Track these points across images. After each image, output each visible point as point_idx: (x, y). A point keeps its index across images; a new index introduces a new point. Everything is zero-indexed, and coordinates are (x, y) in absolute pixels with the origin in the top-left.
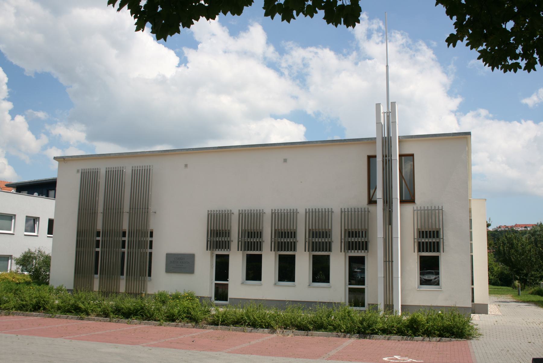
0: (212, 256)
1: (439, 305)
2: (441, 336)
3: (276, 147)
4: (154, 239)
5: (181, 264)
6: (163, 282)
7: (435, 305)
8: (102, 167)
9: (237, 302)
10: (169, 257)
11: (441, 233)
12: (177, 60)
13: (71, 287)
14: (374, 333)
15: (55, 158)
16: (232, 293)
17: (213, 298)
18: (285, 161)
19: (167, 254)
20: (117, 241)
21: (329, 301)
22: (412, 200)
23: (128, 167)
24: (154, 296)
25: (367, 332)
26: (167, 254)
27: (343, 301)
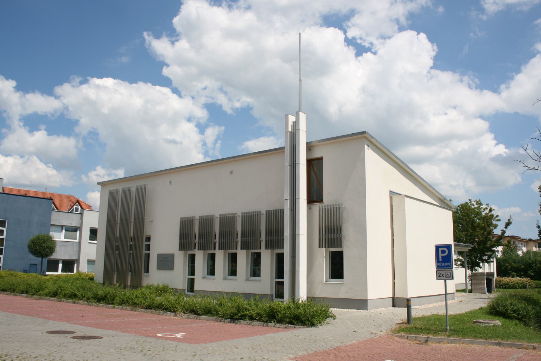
0: (185, 256)
1: (341, 297)
2: (291, 323)
3: (218, 162)
4: (152, 243)
5: (166, 262)
6: (155, 277)
7: (338, 297)
8: (120, 187)
9: (205, 294)
10: (160, 256)
11: (287, 232)
12: (369, 54)
13: (102, 282)
14: (243, 317)
15: (98, 183)
16: (197, 286)
17: (186, 291)
18: (232, 172)
19: (158, 255)
20: (332, 239)
21: (233, 291)
22: (320, 200)
23: (133, 186)
24: (149, 287)
25: (235, 317)
26: (158, 255)
27: (269, 293)
